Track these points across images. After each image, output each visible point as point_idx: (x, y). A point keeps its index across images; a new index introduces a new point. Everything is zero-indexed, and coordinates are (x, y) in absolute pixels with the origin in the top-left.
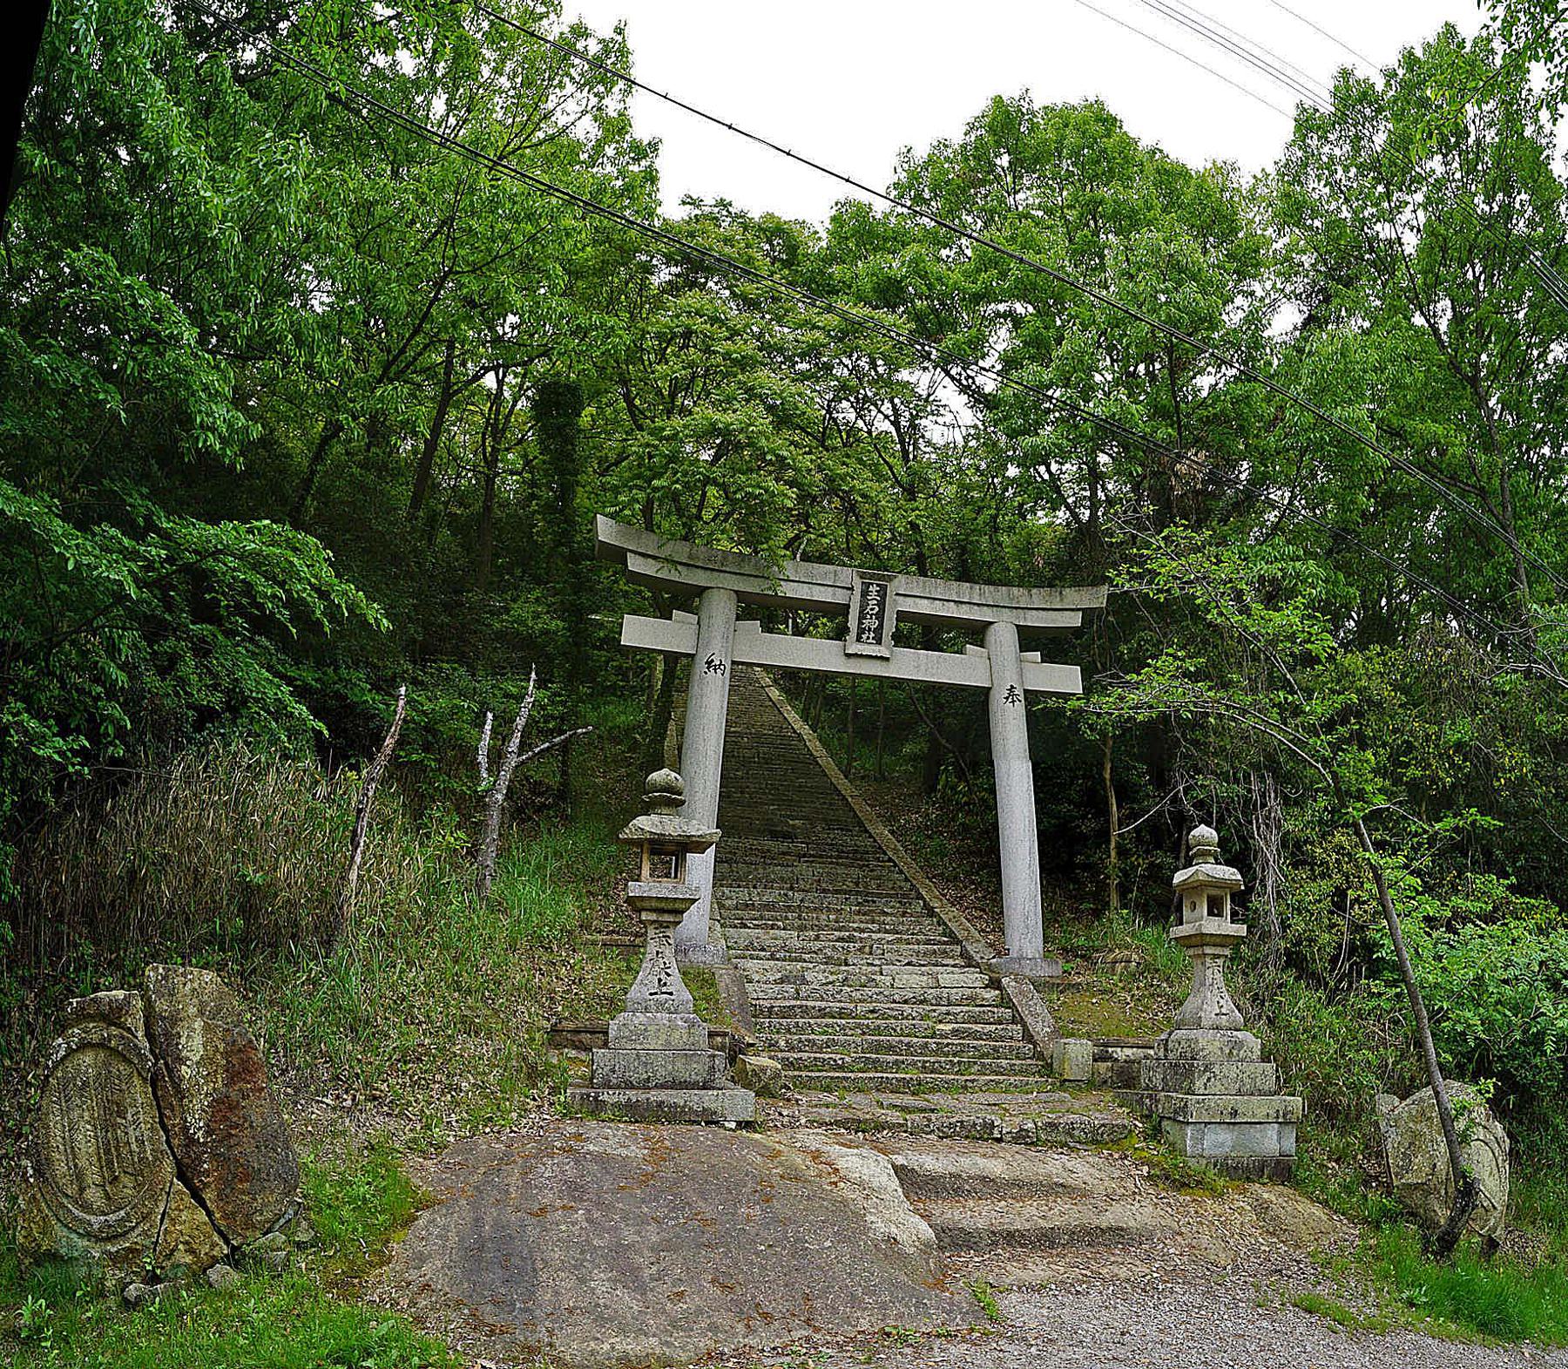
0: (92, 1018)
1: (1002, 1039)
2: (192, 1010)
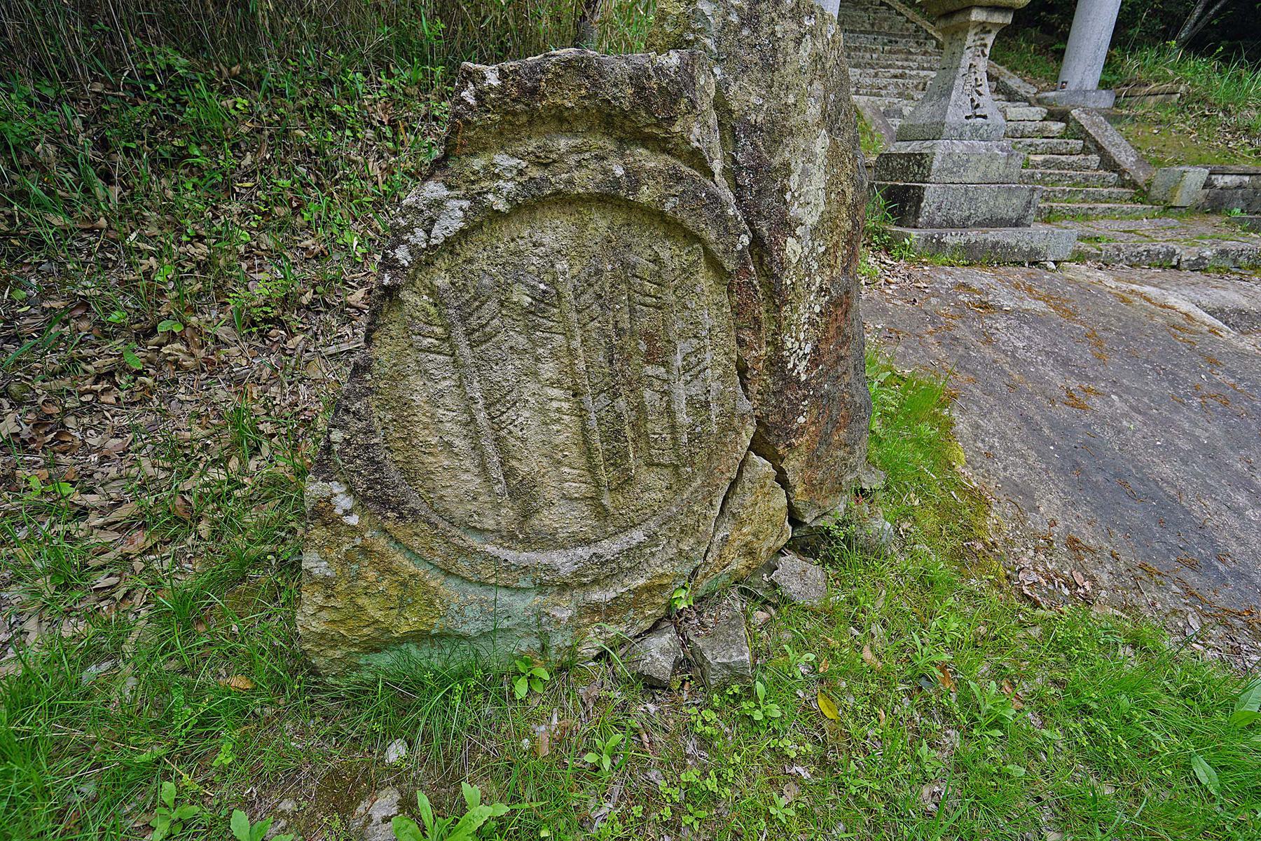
0: (562, 120)
1: (1081, 168)
2: (813, 111)
